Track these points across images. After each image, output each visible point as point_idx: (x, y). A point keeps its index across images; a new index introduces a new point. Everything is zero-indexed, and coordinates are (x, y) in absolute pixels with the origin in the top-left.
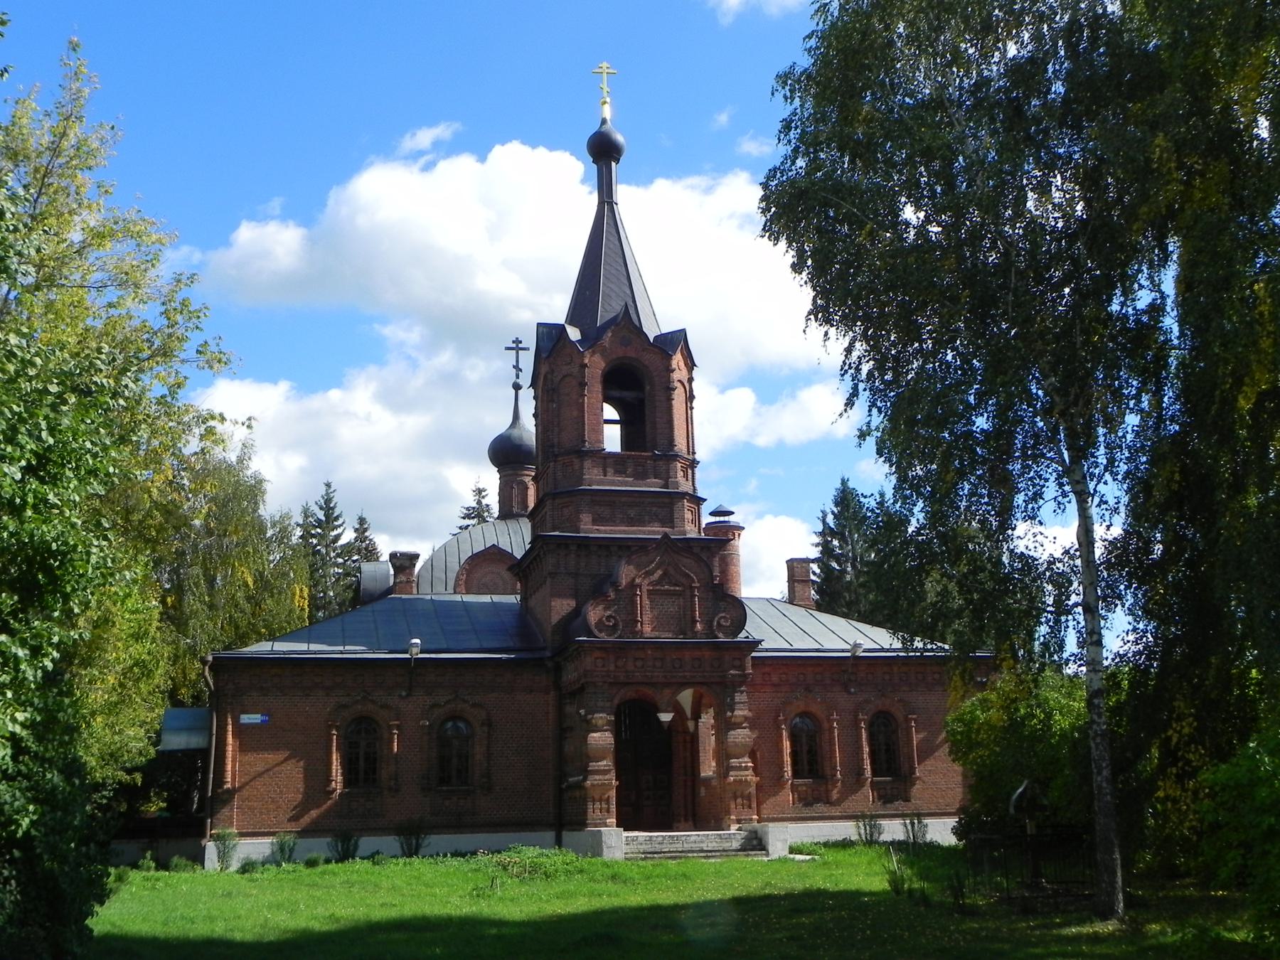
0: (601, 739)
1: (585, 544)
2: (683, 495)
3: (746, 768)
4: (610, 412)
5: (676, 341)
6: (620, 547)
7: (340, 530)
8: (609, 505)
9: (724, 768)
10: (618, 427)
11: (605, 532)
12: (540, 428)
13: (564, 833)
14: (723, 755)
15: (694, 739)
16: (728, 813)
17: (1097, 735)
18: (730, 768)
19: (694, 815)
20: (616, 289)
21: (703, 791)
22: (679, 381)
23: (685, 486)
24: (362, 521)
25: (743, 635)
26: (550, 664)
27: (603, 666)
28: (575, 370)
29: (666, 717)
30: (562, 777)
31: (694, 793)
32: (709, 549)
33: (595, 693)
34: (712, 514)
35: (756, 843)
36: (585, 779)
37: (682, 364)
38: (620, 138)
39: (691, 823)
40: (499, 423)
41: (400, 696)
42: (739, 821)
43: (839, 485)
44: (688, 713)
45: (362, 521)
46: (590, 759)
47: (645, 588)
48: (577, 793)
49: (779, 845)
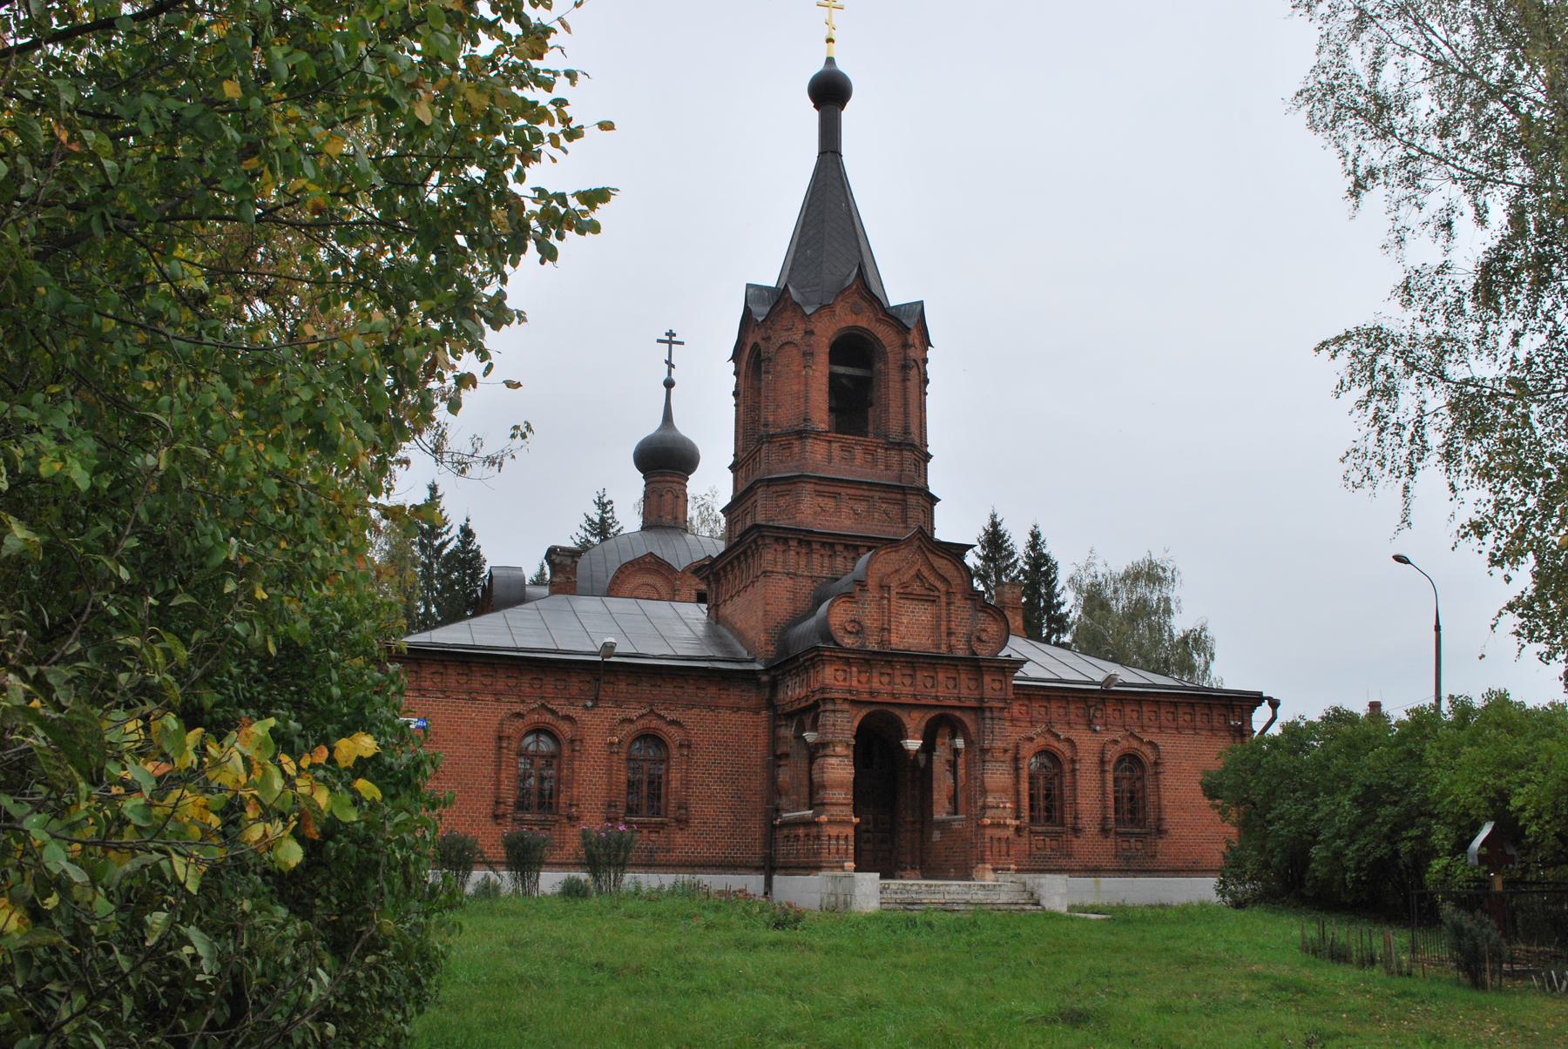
5: (917, 311)
12: (741, 408)
13: (776, 878)
26: (765, 678)
27: (845, 680)
33: (834, 711)
37: (917, 342)
39: (918, 872)
41: (585, 707)
43: (986, 523)
49: (1057, 900)
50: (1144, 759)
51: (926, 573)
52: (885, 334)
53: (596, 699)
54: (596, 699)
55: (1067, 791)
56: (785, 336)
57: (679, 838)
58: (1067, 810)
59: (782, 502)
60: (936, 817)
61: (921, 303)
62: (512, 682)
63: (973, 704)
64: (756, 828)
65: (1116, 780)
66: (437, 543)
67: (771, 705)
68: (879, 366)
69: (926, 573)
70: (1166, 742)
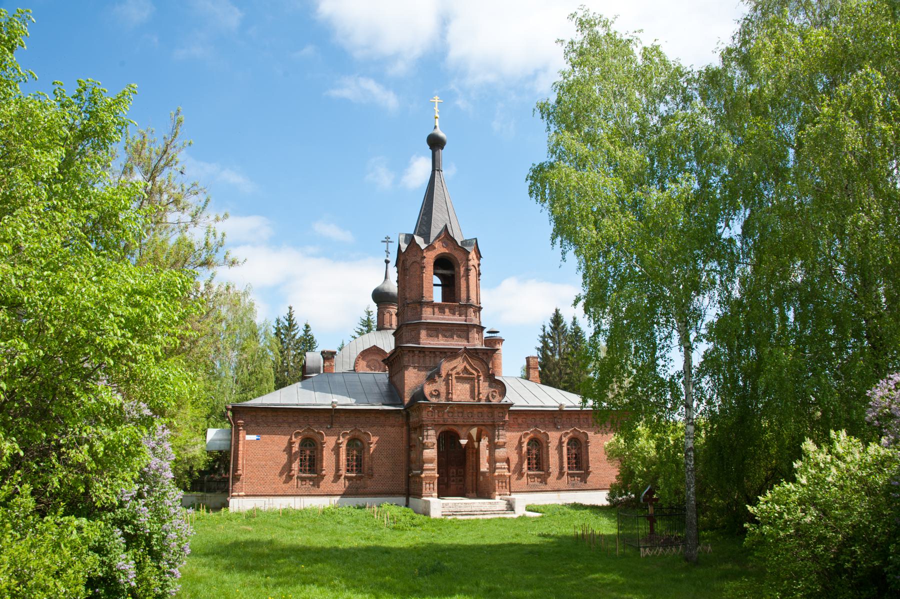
0: (431, 453)
1: (423, 350)
2: (474, 326)
3: (504, 468)
4: (437, 280)
6: (441, 352)
7: (296, 331)
8: (435, 329)
9: (493, 469)
10: (440, 288)
11: (433, 344)
13: (411, 499)
14: (492, 461)
15: (477, 452)
16: (495, 491)
17: (689, 471)
18: (495, 469)
19: (477, 490)
20: (441, 216)
21: (481, 478)
22: (473, 266)
23: (475, 321)
24: (307, 326)
25: (505, 399)
28: (419, 259)
29: (464, 442)
30: (409, 470)
31: (477, 479)
32: (487, 354)
34: (488, 332)
35: (511, 507)
36: (422, 473)
37: (475, 257)
38: (441, 134)
40: (377, 282)
42: (500, 495)
43: (554, 312)
44: (475, 438)
45: (307, 326)
46: (424, 463)
47: (454, 376)
48: (418, 480)
50: (581, 440)
51: (468, 367)
52: (458, 255)
53: (332, 424)
54: (332, 424)
55: (545, 456)
56: (414, 259)
57: (369, 482)
58: (545, 464)
59: (413, 333)
60: (482, 470)
61: (476, 239)
62: (295, 419)
63: (491, 423)
64: (403, 477)
65: (568, 449)
66: (293, 333)
67: (407, 423)
68: (457, 269)
69: (468, 367)
70: (590, 434)
